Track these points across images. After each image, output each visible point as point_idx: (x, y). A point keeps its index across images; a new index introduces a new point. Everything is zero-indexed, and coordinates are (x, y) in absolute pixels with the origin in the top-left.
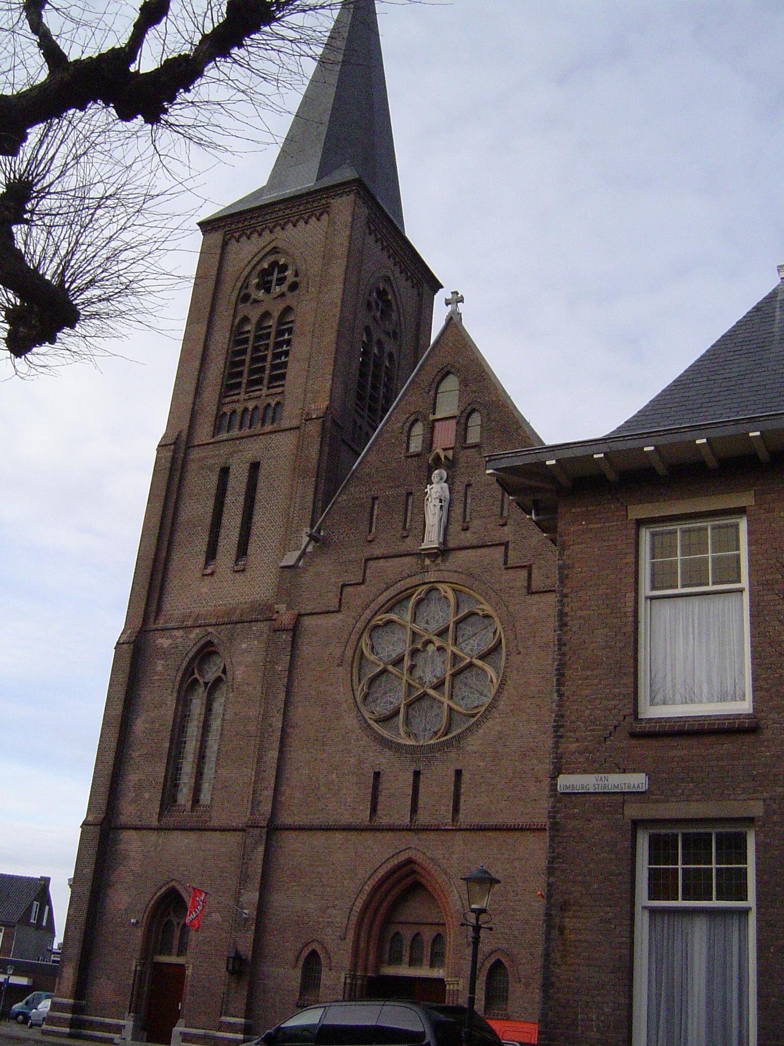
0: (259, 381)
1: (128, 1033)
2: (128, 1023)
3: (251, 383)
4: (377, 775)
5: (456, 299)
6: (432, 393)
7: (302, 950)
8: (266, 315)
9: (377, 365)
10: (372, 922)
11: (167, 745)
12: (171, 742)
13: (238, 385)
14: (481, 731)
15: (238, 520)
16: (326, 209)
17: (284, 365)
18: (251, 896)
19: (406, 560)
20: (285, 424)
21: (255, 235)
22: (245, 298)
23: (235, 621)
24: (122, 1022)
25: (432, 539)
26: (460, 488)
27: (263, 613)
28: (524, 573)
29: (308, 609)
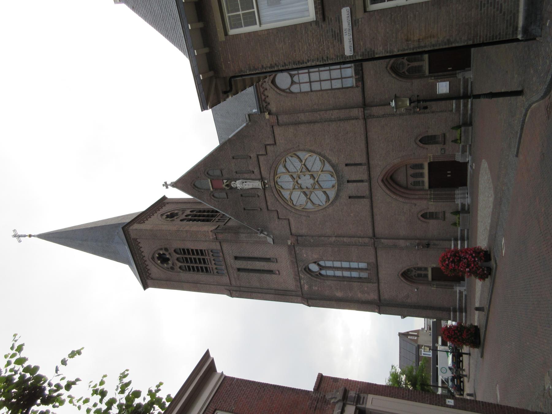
0: (204, 259)
1: (462, 289)
2: (458, 289)
3: (205, 263)
4: (350, 197)
5: (166, 185)
6: (202, 191)
7: (421, 221)
8: (178, 259)
9: (195, 216)
10: (408, 194)
11: (345, 283)
12: (344, 281)
13: (206, 268)
14: (330, 157)
15: (257, 263)
16: (135, 240)
17: (197, 250)
18: (402, 243)
19: (267, 195)
20: (219, 248)
21: (147, 267)
22: (172, 268)
23: (296, 259)
24: (458, 291)
25: (257, 184)
26: (238, 175)
27: (292, 249)
28: (268, 147)
29: (289, 231)
